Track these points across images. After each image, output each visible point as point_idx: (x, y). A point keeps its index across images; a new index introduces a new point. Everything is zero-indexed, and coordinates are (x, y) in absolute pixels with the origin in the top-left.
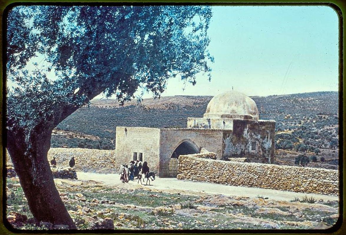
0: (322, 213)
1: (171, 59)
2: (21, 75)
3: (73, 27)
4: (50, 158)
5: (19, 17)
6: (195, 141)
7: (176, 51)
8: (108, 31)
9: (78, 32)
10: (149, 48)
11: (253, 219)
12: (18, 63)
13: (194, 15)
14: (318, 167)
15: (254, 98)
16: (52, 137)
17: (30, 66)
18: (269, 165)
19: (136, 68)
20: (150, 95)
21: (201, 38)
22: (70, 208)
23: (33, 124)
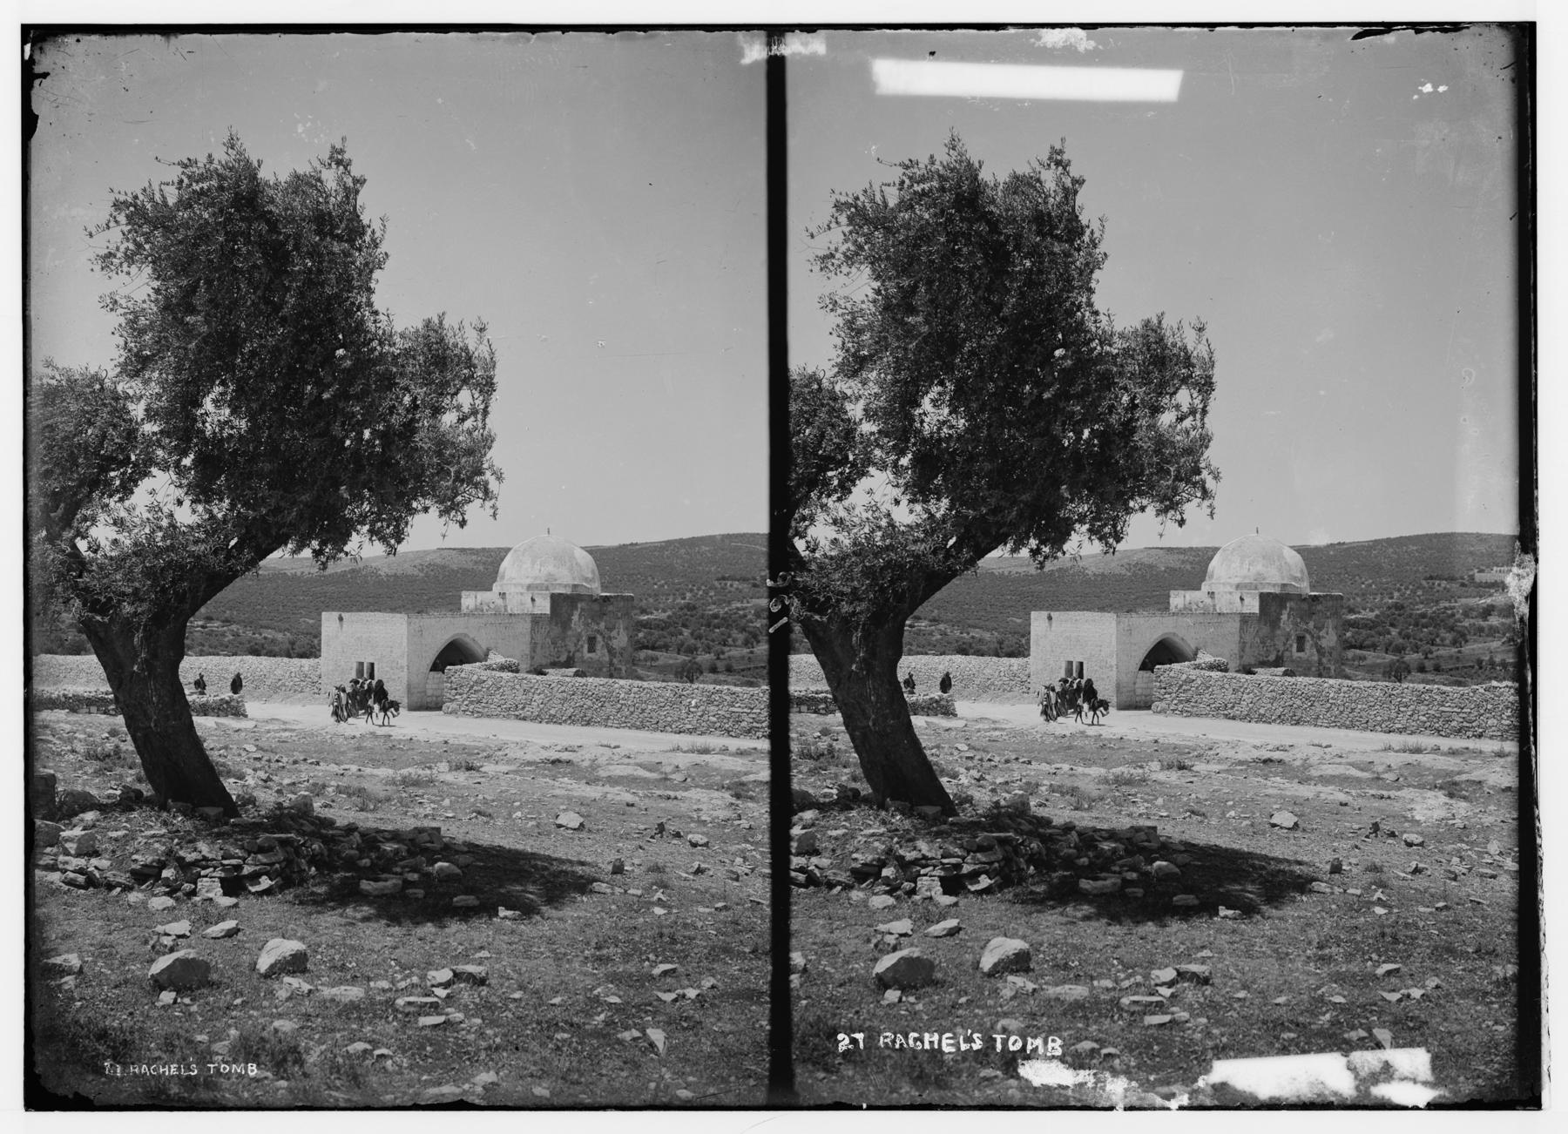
0: (1438, 774)
1: (1136, 477)
2: (842, 514)
3: (941, 418)
4: (901, 676)
5: (835, 399)
6: (478, 637)
7: (1145, 460)
8: (1010, 425)
9: (232, 428)
10: (1091, 454)
11: (588, 788)
12: (835, 491)
13: (1178, 389)
14: (720, 683)
15: (592, 551)
16: (906, 634)
17: (141, 496)
18: (1332, 681)
19: (1067, 495)
20: (1097, 547)
21: (1193, 433)
22: (229, 774)
23: (868, 610)
